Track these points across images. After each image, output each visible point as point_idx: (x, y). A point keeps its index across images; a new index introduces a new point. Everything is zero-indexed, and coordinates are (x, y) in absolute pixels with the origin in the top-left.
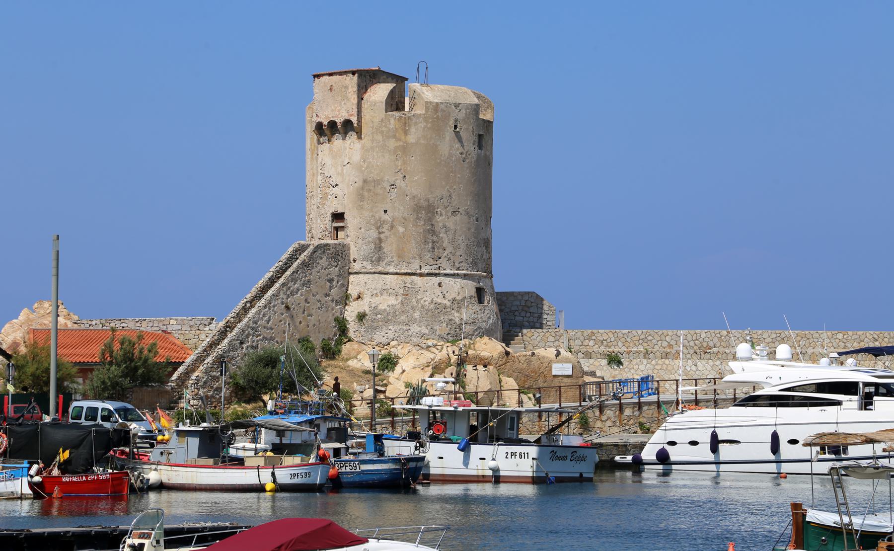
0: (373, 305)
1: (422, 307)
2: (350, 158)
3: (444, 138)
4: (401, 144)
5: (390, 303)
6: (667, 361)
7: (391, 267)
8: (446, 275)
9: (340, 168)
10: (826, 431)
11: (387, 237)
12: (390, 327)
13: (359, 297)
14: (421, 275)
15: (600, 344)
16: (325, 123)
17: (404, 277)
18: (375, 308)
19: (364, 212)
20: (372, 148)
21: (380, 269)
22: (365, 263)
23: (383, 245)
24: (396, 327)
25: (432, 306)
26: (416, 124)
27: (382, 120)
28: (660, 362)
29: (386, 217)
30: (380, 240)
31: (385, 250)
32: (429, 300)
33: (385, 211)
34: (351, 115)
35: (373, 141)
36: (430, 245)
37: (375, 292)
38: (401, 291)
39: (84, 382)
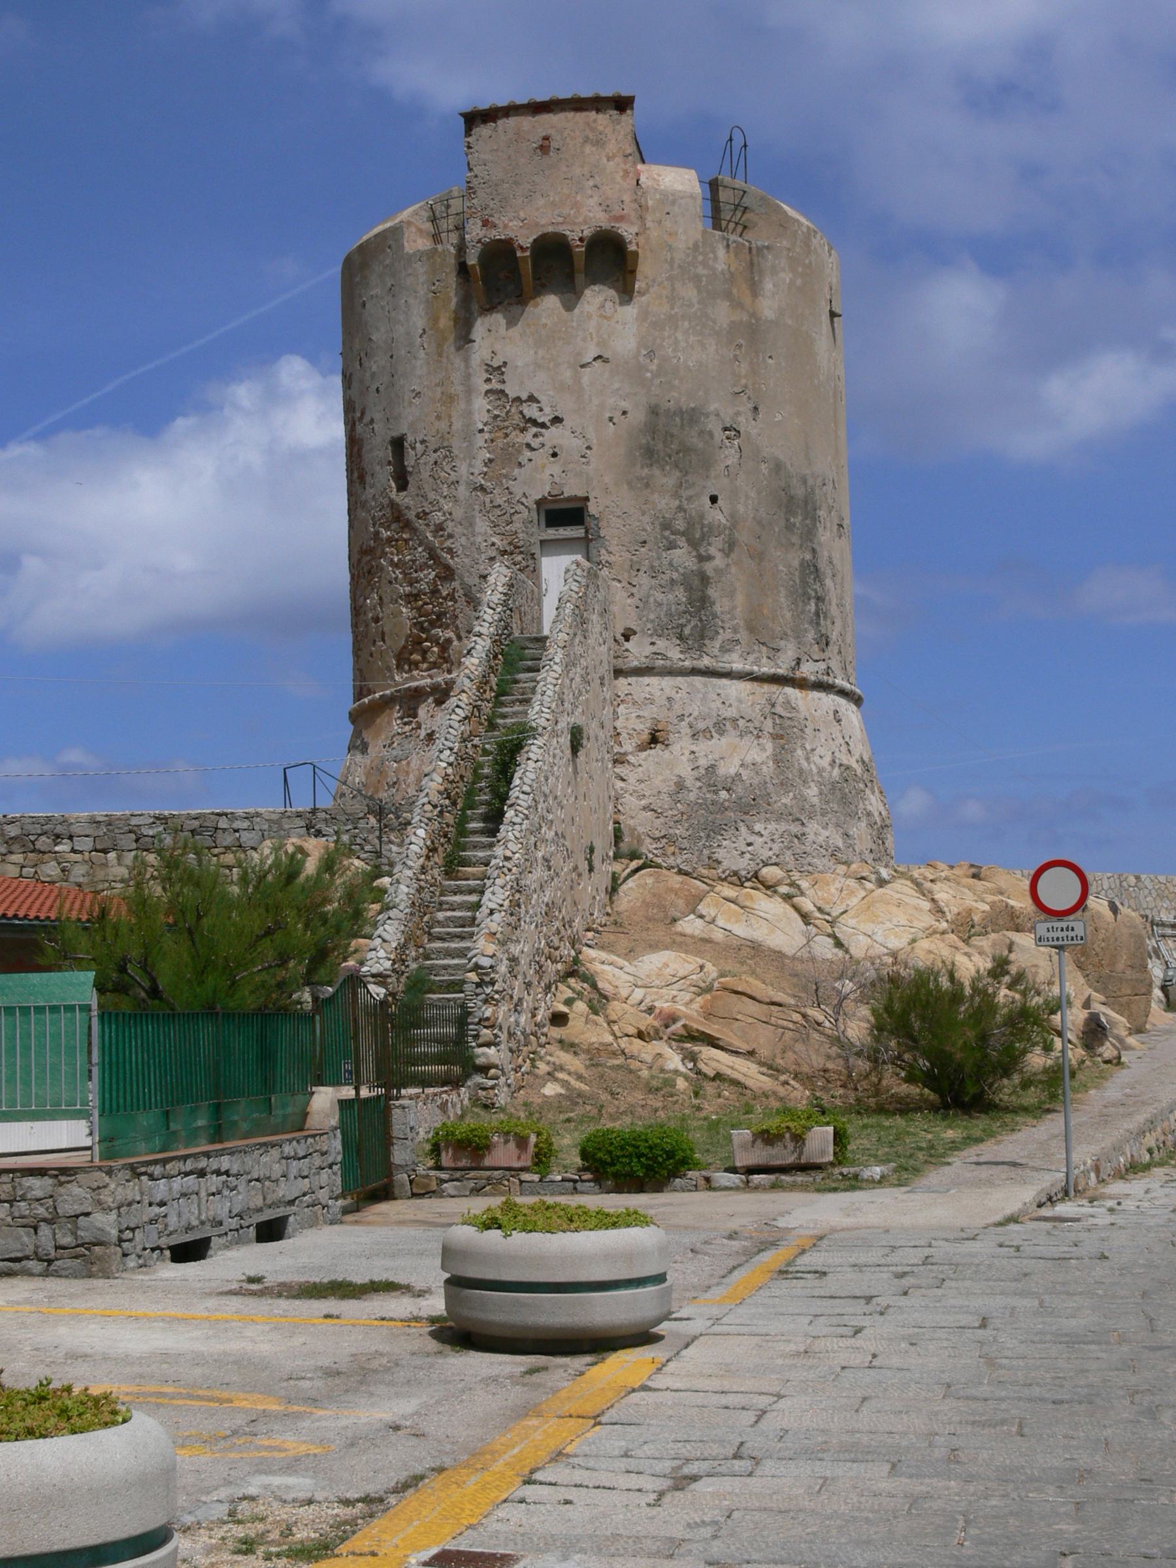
0: (703, 762)
2: (602, 343)
4: (745, 318)
5: (749, 759)
7: (735, 656)
9: (567, 374)
10: (25, 1126)
12: (758, 827)
13: (654, 739)
14: (802, 684)
17: (766, 687)
21: (706, 662)
22: (661, 644)
23: (711, 592)
24: (772, 826)
27: (696, 246)
29: (716, 516)
30: (704, 579)
31: (717, 608)
32: (828, 759)
33: (714, 499)
34: (621, 218)
35: (672, 299)
36: (812, 607)
37: (701, 725)
38: (768, 725)
39: (334, 949)
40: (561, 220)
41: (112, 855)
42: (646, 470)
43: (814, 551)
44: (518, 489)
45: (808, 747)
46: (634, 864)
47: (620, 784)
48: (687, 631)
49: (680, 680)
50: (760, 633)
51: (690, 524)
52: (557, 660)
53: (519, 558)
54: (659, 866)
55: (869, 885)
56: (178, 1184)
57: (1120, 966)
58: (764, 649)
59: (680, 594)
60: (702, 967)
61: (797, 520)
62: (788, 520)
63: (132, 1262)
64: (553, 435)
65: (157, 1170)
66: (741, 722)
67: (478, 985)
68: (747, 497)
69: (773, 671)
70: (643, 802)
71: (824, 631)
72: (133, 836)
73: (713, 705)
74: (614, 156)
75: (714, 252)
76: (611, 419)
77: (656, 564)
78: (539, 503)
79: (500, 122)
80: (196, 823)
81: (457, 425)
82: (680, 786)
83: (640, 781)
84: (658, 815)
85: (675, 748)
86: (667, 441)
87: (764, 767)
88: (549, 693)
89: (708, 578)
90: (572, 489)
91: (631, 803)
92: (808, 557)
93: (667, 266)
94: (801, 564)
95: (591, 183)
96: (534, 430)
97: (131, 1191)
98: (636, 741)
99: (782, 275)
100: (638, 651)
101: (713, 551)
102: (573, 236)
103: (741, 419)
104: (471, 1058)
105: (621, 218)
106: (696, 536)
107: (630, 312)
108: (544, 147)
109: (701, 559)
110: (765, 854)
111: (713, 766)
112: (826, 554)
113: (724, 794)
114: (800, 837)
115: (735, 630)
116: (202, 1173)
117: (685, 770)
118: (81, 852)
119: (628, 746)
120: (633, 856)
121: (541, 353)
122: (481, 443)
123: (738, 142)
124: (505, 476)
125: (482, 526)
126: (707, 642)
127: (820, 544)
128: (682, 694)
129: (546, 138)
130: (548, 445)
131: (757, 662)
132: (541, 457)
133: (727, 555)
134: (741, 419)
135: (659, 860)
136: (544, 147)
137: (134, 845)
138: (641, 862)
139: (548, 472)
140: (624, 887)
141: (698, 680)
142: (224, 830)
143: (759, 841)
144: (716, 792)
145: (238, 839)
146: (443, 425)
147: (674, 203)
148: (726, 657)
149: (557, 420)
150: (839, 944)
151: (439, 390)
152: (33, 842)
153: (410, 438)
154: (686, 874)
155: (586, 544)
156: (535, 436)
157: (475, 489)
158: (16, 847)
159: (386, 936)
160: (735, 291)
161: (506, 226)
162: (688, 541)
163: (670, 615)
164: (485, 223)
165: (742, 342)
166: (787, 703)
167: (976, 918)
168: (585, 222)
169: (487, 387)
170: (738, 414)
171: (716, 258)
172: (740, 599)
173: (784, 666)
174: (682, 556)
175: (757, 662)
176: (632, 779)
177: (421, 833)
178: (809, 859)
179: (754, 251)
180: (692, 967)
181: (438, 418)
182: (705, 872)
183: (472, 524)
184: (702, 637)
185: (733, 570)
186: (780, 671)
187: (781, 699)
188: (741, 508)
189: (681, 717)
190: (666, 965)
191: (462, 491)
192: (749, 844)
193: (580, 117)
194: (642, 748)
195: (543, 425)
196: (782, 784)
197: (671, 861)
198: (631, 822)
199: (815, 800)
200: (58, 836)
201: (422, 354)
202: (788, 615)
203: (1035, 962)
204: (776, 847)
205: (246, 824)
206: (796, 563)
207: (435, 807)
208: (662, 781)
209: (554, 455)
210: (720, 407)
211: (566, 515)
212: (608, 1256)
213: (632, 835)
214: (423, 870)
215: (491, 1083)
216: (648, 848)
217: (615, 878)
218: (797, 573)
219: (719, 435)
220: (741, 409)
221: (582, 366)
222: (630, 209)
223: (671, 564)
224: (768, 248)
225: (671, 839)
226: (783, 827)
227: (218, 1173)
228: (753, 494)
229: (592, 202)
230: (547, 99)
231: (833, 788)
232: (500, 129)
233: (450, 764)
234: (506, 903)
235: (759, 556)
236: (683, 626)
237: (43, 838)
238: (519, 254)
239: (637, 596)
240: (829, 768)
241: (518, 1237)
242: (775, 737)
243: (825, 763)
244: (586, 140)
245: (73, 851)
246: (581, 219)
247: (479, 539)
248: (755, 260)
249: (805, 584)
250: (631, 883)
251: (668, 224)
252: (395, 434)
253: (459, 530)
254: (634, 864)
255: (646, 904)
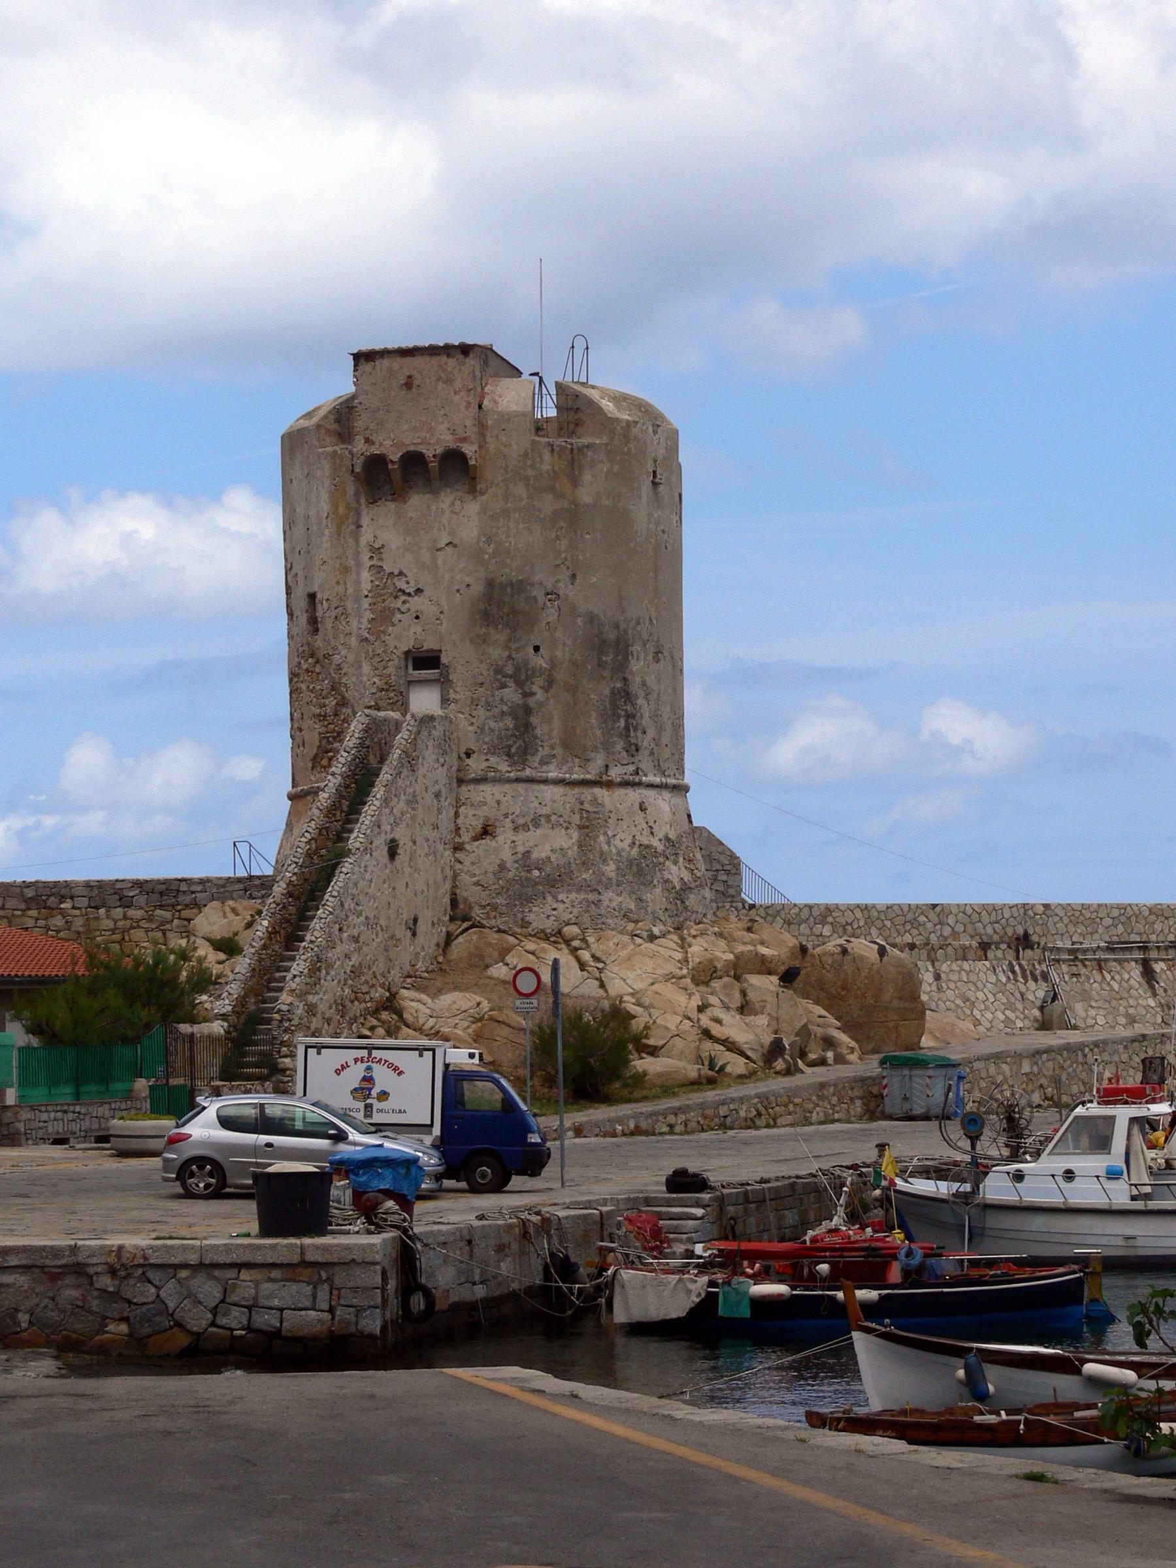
0: (521, 849)
1: (619, 853)
2: (452, 533)
3: (640, 497)
5: (557, 846)
6: (966, 966)
7: (551, 767)
8: (651, 786)
9: (426, 556)
11: (540, 704)
12: (561, 897)
14: (609, 785)
15: (840, 931)
16: (395, 456)
18: (527, 854)
19: (490, 650)
20: (506, 513)
21: (528, 772)
22: (493, 760)
23: (534, 720)
24: (573, 896)
25: (635, 852)
26: (593, 464)
27: (526, 453)
28: (954, 967)
29: (540, 662)
30: (528, 711)
31: (538, 732)
32: (629, 840)
33: (537, 649)
34: (464, 440)
36: (622, 723)
37: (521, 821)
38: (576, 819)
40: (419, 441)
41: (102, 911)
42: (484, 629)
43: (625, 679)
44: (391, 643)
45: (610, 833)
46: (465, 925)
47: (459, 866)
48: (513, 750)
49: (507, 787)
50: (572, 747)
51: (517, 669)
52: (378, 796)
53: (392, 695)
54: (483, 926)
55: (638, 941)
56: (52, 1115)
57: (886, 997)
58: (577, 760)
59: (509, 722)
60: (478, 1004)
61: (607, 658)
62: (600, 659)
63: (30, 1142)
64: (416, 602)
65: (43, 1109)
66: (553, 818)
67: (281, 1021)
68: (564, 645)
69: (582, 776)
70: (475, 879)
71: (633, 741)
72: (117, 897)
73: (532, 806)
74: (460, 391)
75: (541, 457)
76: (458, 591)
77: (490, 700)
78: (407, 654)
79: (378, 362)
80: (164, 887)
81: (350, 591)
82: (502, 867)
83: (473, 864)
84: (485, 888)
85: (500, 839)
86: (501, 606)
87: (570, 852)
88: (367, 822)
89: (531, 709)
90: (430, 644)
91: (465, 878)
92: (619, 685)
93: (502, 471)
94: (612, 692)
95: (442, 412)
96: (404, 598)
97: (30, 1115)
98: (472, 833)
99: (600, 466)
100: (476, 765)
101: (535, 688)
102: (429, 453)
103: (561, 585)
104: (276, 1064)
105: (464, 440)
106: (522, 677)
107: (472, 508)
108: (409, 384)
109: (526, 695)
110: (566, 916)
111: (528, 852)
112: (638, 679)
113: (536, 873)
114: (597, 904)
115: (552, 748)
116: (65, 1112)
117: (507, 856)
118: (79, 909)
119: (466, 837)
120: (465, 919)
121: (408, 539)
122: (366, 605)
123: (580, 345)
124: (384, 632)
125: (366, 669)
126: (529, 757)
127: (631, 672)
128: (508, 797)
129: (410, 377)
130: (413, 610)
131: (570, 771)
132: (408, 619)
133: (547, 692)
134: (561, 585)
135: (484, 922)
136: (409, 384)
137: (118, 903)
138: (470, 923)
139: (412, 631)
140: (456, 942)
141: (521, 787)
142: (184, 892)
143: (561, 907)
144: (529, 871)
145: (195, 899)
146: (341, 589)
147: (508, 421)
148: (545, 768)
149: (419, 591)
150: (602, 985)
151: (338, 562)
152: (45, 901)
153: (319, 596)
154: (504, 932)
155: (444, 682)
156: (404, 602)
157: (362, 641)
158: (33, 905)
159: (232, 991)
160: (557, 486)
161: (381, 444)
162: (515, 682)
163: (500, 738)
164: (367, 440)
165: (562, 524)
166: (595, 801)
167: (719, 966)
168: (437, 442)
169: (371, 563)
170: (558, 581)
171: (542, 461)
172: (557, 723)
173: (593, 772)
174: (511, 693)
175: (570, 771)
176: (467, 863)
177: (265, 923)
178: (604, 919)
179: (575, 452)
180: (470, 1004)
181: (338, 583)
182: (519, 930)
183: (360, 667)
184: (525, 754)
185: (552, 701)
186: (588, 777)
187: (589, 798)
188: (559, 654)
189: (506, 816)
190: (454, 1002)
191: (353, 641)
192: (554, 909)
193: (435, 361)
194: (476, 838)
195: (409, 594)
196: (583, 864)
197: (493, 922)
198: (465, 894)
199: (613, 875)
200: (63, 897)
201: (327, 532)
202: (598, 732)
203: (764, 998)
204: (575, 911)
205: (199, 888)
206: (607, 691)
207: (278, 905)
208: (489, 865)
209: (417, 617)
210: (543, 577)
211: (426, 661)
212: (154, 1127)
213: (465, 903)
214: (264, 947)
215: (286, 1079)
216: (477, 913)
217: (449, 934)
218: (607, 700)
219: (541, 599)
220: (561, 577)
221: (438, 550)
222: (472, 431)
223: (502, 700)
224: (588, 446)
225: (494, 907)
226: (583, 896)
227: (74, 1112)
228: (569, 643)
229: (443, 427)
230: (411, 346)
231: (631, 864)
232: (378, 367)
233: (295, 874)
234: (306, 971)
235: (573, 689)
236: (510, 746)
237: (52, 899)
238: (390, 466)
239: (476, 724)
240: (628, 849)
241: (128, 1122)
242: (581, 827)
243: (625, 845)
244: (439, 379)
245: (74, 908)
246: (434, 443)
247: (365, 679)
248: (576, 458)
249: (614, 706)
250: (461, 939)
251: (503, 438)
252: (312, 591)
253: (351, 670)
254: (465, 925)
255: (471, 955)
